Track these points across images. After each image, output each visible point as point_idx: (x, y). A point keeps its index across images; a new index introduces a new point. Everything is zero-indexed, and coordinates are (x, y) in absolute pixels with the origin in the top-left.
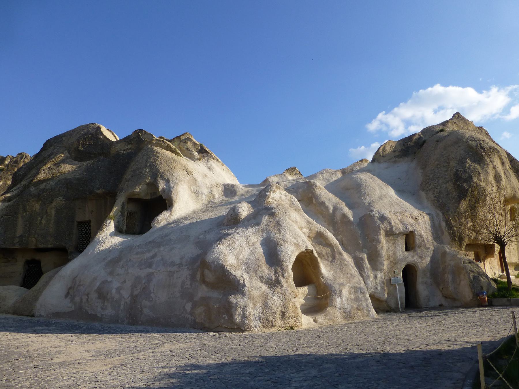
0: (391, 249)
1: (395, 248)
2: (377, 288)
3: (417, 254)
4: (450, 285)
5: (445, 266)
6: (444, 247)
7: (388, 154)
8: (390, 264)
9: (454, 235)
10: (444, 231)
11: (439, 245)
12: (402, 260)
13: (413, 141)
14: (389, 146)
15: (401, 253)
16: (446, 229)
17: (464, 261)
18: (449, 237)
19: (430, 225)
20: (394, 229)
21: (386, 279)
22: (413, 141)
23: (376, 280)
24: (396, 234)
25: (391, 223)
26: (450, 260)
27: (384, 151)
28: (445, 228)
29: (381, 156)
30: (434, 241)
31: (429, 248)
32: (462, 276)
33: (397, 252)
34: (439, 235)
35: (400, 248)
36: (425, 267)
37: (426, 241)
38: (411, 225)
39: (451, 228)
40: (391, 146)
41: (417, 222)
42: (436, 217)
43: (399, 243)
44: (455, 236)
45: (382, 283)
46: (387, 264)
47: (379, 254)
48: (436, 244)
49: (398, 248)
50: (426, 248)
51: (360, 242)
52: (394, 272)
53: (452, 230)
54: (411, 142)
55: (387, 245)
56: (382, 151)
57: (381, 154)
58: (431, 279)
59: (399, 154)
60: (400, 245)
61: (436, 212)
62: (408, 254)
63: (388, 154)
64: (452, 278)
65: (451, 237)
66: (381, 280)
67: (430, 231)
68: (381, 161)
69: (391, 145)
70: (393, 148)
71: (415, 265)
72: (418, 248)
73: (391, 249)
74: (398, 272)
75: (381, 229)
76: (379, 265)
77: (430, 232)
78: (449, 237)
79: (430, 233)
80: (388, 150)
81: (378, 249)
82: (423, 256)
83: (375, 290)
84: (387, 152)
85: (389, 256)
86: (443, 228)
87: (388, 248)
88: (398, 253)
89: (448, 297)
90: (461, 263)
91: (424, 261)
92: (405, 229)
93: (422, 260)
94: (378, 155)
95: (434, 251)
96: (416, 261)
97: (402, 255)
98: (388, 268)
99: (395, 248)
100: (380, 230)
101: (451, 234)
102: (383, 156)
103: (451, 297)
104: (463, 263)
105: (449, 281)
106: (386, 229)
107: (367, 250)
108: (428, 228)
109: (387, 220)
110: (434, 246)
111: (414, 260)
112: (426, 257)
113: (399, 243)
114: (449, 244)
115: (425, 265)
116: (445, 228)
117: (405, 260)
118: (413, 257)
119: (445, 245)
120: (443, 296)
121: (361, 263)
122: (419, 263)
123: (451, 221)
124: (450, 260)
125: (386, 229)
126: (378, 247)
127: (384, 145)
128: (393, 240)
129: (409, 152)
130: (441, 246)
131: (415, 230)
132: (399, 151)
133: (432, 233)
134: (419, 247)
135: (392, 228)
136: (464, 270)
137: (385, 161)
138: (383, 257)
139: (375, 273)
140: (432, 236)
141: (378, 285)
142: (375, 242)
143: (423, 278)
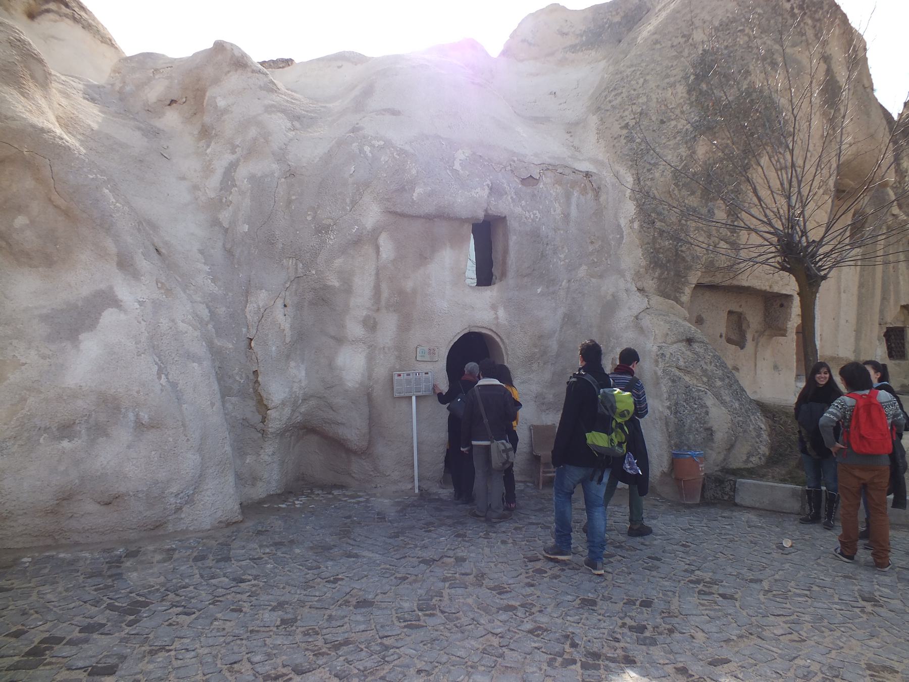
132: (578, 35)
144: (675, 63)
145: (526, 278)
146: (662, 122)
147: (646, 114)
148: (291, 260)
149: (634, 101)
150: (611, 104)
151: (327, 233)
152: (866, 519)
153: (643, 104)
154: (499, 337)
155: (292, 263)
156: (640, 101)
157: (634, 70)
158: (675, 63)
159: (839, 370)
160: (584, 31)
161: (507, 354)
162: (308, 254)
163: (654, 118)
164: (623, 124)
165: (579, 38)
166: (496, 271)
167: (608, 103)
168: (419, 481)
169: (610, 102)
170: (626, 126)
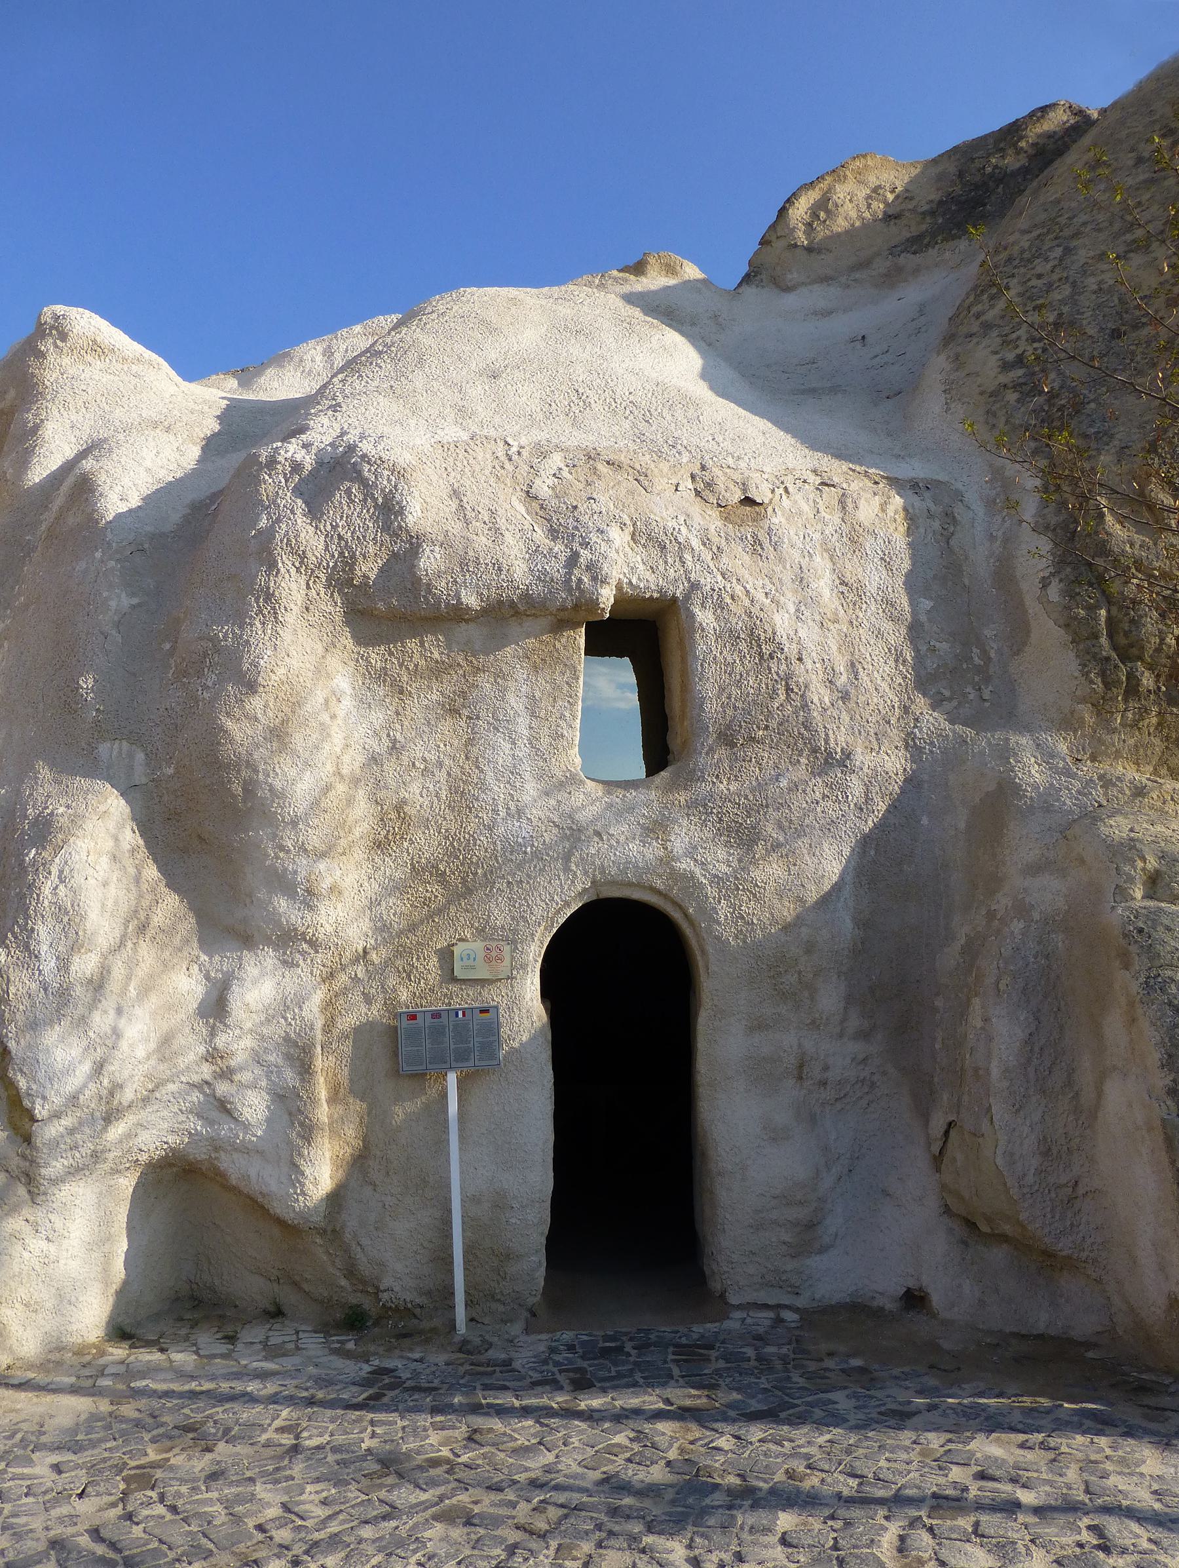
0: (418, 750)
1: (470, 742)
2: (224, 1107)
3: (700, 807)
4: (999, 1110)
5: (991, 915)
6: (1005, 753)
7: (850, 233)
8: (398, 888)
9: (1123, 641)
10: (1033, 607)
11: (969, 732)
12: (537, 855)
13: (1023, 144)
14: (865, 192)
15: (530, 790)
16: (1054, 592)
17: (1157, 872)
18: (1074, 667)
19: (906, 565)
20: (430, 561)
21: (347, 1021)
22: (1023, 144)
23: (213, 1034)
24: (458, 614)
25: (401, 512)
26: (1034, 869)
27: (822, 215)
28: (1045, 587)
29: (796, 246)
30: (921, 704)
31: (847, 755)
32: (1114, 1026)
33: (490, 776)
34: (984, 653)
35: (523, 751)
36: (786, 928)
37: (819, 694)
38: (663, 548)
39: (1100, 581)
40: (875, 190)
41: (748, 531)
42: (980, 510)
43: (515, 703)
44: (1128, 652)
45: (288, 1057)
46: (372, 889)
47: (250, 788)
48: (931, 720)
49: (507, 746)
50: (815, 751)
51: (87, 683)
52: (446, 956)
53: (1109, 601)
54: (1010, 151)
55: (378, 717)
56: (807, 218)
57: (801, 234)
58: (864, 1035)
59: (924, 227)
60: (522, 725)
61: (997, 473)
62: (610, 806)
63: (847, 232)
64: (1029, 1041)
65: (1089, 656)
66: (277, 1030)
67: (892, 619)
68: (793, 277)
69: (873, 180)
70: (890, 197)
71: (675, 904)
72: (722, 752)
73: (418, 750)
74: (488, 959)
75: (285, 562)
76: (261, 895)
77: (887, 626)
78: (1068, 662)
79: (896, 635)
80: (853, 214)
81: (232, 741)
82: (770, 829)
83: (209, 1122)
84: (840, 225)
85: (403, 818)
86: (1029, 587)
87: (386, 742)
88: (499, 790)
89: (985, 1228)
90: (1121, 893)
91: (770, 872)
92: (556, 568)
93: (748, 860)
94: (779, 245)
95: (912, 782)
96: (685, 865)
97: (535, 813)
98: (381, 928)
99: (470, 742)
100: (272, 565)
101: (1096, 636)
102: (809, 250)
103: (1007, 1228)
104: (1138, 894)
105: (988, 1072)
106: (348, 562)
107: (140, 756)
108: (872, 588)
109: (363, 482)
110: (911, 744)
111: (668, 860)
112: (800, 832)
113: (515, 703)
114: (1068, 723)
115: (787, 911)
116: (1045, 587)
117: (567, 858)
118: (657, 829)
119: (1027, 728)
120: (947, 1211)
121: (20, 857)
122: (711, 891)
123: (1109, 518)
124: (1034, 869)
125: (348, 562)
126: (229, 724)
127: (824, 185)
128: (437, 671)
129: (984, 205)
130: (982, 742)
131: (695, 586)
132: (923, 213)
133: (915, 631)
134: (727, 738)
135: (414, 545)
136: (1127, 966)
137: (825, 279)
138: (294, 823)
139: (219, 964)
140: (909, 655)
141: (245, 1077)
142: (211, 679)
143: (758, 1026)
144: (1146, 197)
145: (862, 788)
146: (1116, 334)
147: (1072, 323)
148: (116, 746)
149: (1041, 301)
150: (981, 320)
151: (200, 674)
152: (1120, 1507)
153: (1063, 302)
154: (680, 907)
155: (120, 752)
156: (1056, 296)
157: (1039, 236)
158: (1146, 197)
159: (1034, 637)
160: (941, 203)
161: (703, 952)
162: (159, 730)
163: (1091, 331)
164: (1010, 356)
165: (928, 219)
166: (674, 743)
167: (973, 319)
168: (469, 1304)
169: (978, 316)
170: (1020, 360)
